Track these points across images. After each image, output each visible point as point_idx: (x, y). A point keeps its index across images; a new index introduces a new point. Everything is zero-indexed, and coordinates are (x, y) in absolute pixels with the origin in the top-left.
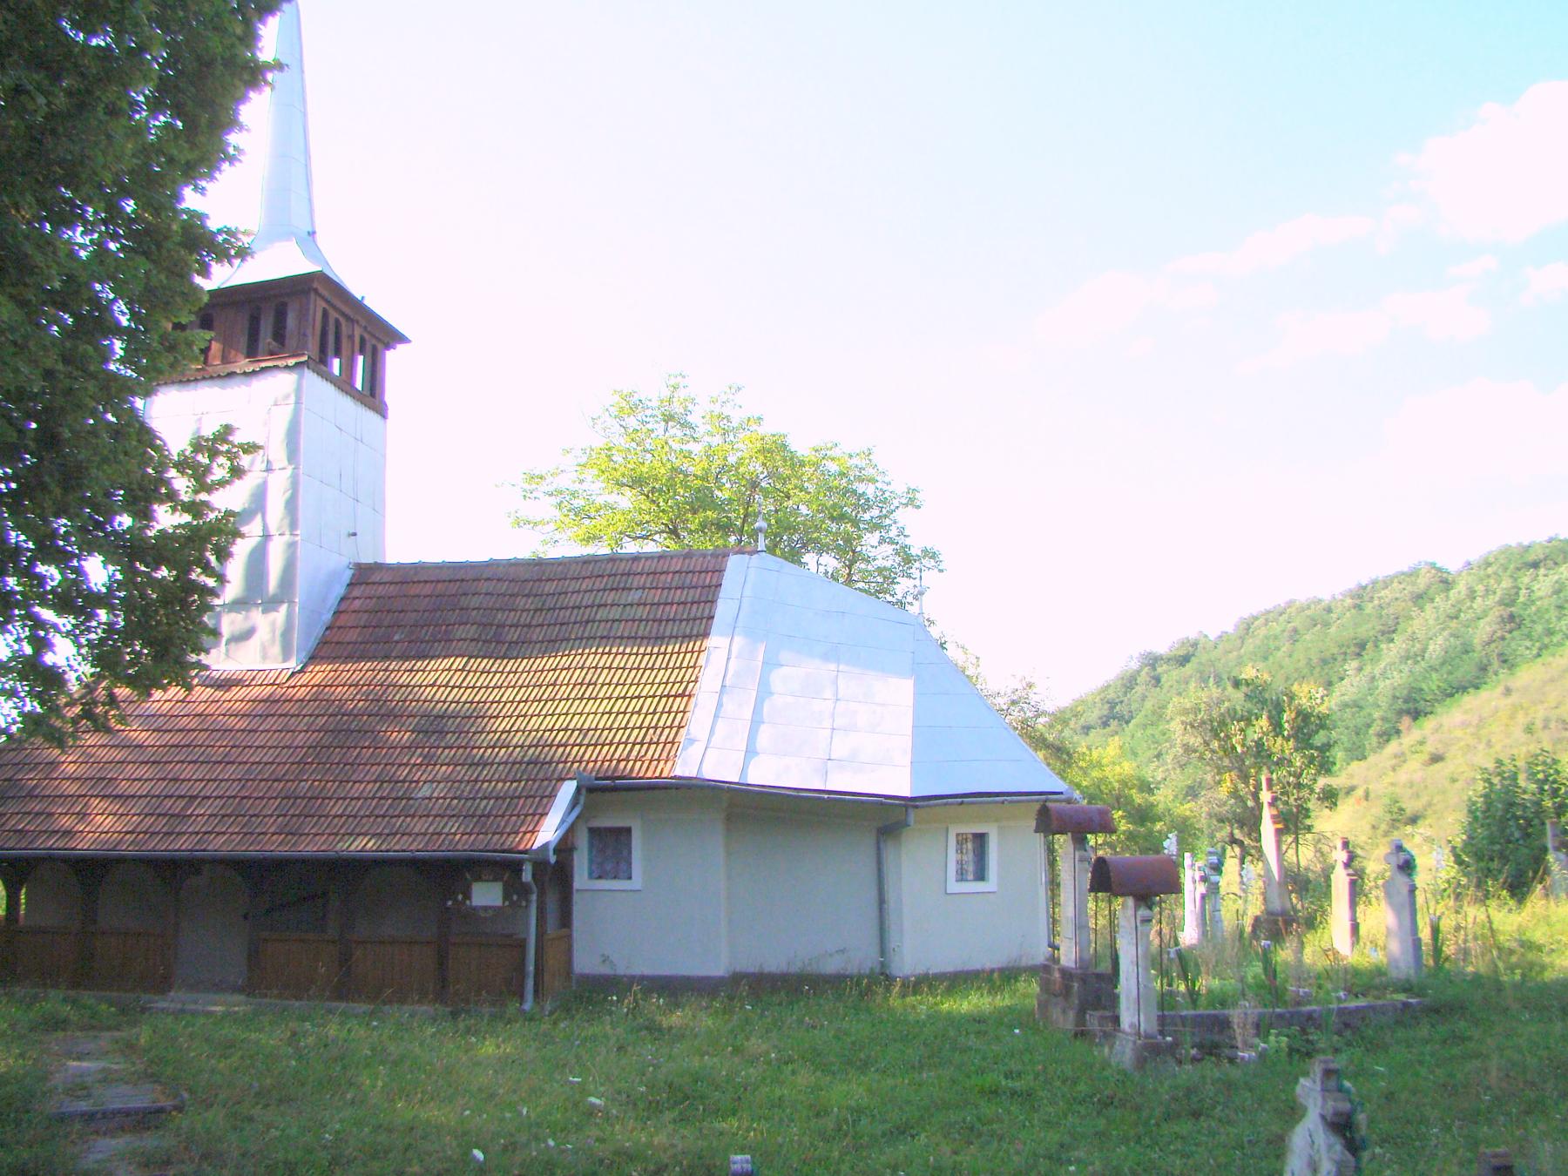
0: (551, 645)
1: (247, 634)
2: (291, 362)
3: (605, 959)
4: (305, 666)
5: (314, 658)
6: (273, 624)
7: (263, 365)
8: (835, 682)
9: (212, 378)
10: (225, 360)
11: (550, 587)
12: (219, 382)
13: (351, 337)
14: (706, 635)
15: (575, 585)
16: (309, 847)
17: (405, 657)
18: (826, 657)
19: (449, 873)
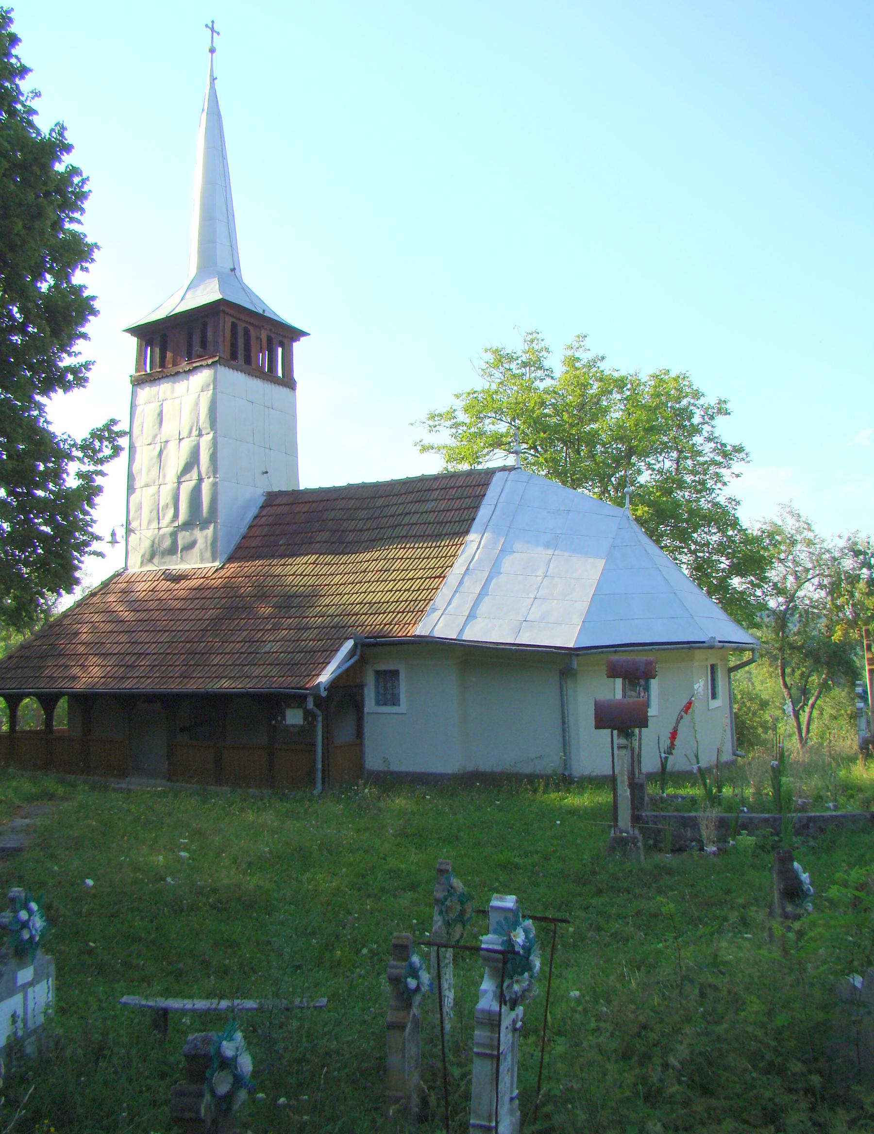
0: (371, 544)
1: (191, 545)
2: (210, 362)
3: (385, 760)
4: (224, 565)
5: (231, 559)
6: (206, 537)
7: (195, 365)
8: (548, 564)
9: (167, 376)
10: (175, 364)
11: (379, 502)
12: (171, 378)
13: (259, 338)
14: (467, 532)
15: (395, 500)
16: (192, 686)
17: (282, 556)
18: (547, 546)
19: (272, 703)
